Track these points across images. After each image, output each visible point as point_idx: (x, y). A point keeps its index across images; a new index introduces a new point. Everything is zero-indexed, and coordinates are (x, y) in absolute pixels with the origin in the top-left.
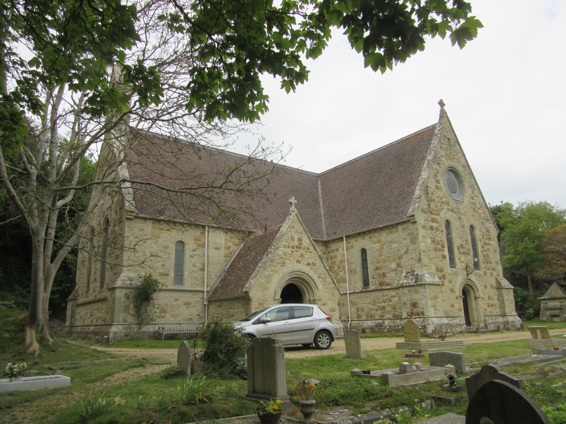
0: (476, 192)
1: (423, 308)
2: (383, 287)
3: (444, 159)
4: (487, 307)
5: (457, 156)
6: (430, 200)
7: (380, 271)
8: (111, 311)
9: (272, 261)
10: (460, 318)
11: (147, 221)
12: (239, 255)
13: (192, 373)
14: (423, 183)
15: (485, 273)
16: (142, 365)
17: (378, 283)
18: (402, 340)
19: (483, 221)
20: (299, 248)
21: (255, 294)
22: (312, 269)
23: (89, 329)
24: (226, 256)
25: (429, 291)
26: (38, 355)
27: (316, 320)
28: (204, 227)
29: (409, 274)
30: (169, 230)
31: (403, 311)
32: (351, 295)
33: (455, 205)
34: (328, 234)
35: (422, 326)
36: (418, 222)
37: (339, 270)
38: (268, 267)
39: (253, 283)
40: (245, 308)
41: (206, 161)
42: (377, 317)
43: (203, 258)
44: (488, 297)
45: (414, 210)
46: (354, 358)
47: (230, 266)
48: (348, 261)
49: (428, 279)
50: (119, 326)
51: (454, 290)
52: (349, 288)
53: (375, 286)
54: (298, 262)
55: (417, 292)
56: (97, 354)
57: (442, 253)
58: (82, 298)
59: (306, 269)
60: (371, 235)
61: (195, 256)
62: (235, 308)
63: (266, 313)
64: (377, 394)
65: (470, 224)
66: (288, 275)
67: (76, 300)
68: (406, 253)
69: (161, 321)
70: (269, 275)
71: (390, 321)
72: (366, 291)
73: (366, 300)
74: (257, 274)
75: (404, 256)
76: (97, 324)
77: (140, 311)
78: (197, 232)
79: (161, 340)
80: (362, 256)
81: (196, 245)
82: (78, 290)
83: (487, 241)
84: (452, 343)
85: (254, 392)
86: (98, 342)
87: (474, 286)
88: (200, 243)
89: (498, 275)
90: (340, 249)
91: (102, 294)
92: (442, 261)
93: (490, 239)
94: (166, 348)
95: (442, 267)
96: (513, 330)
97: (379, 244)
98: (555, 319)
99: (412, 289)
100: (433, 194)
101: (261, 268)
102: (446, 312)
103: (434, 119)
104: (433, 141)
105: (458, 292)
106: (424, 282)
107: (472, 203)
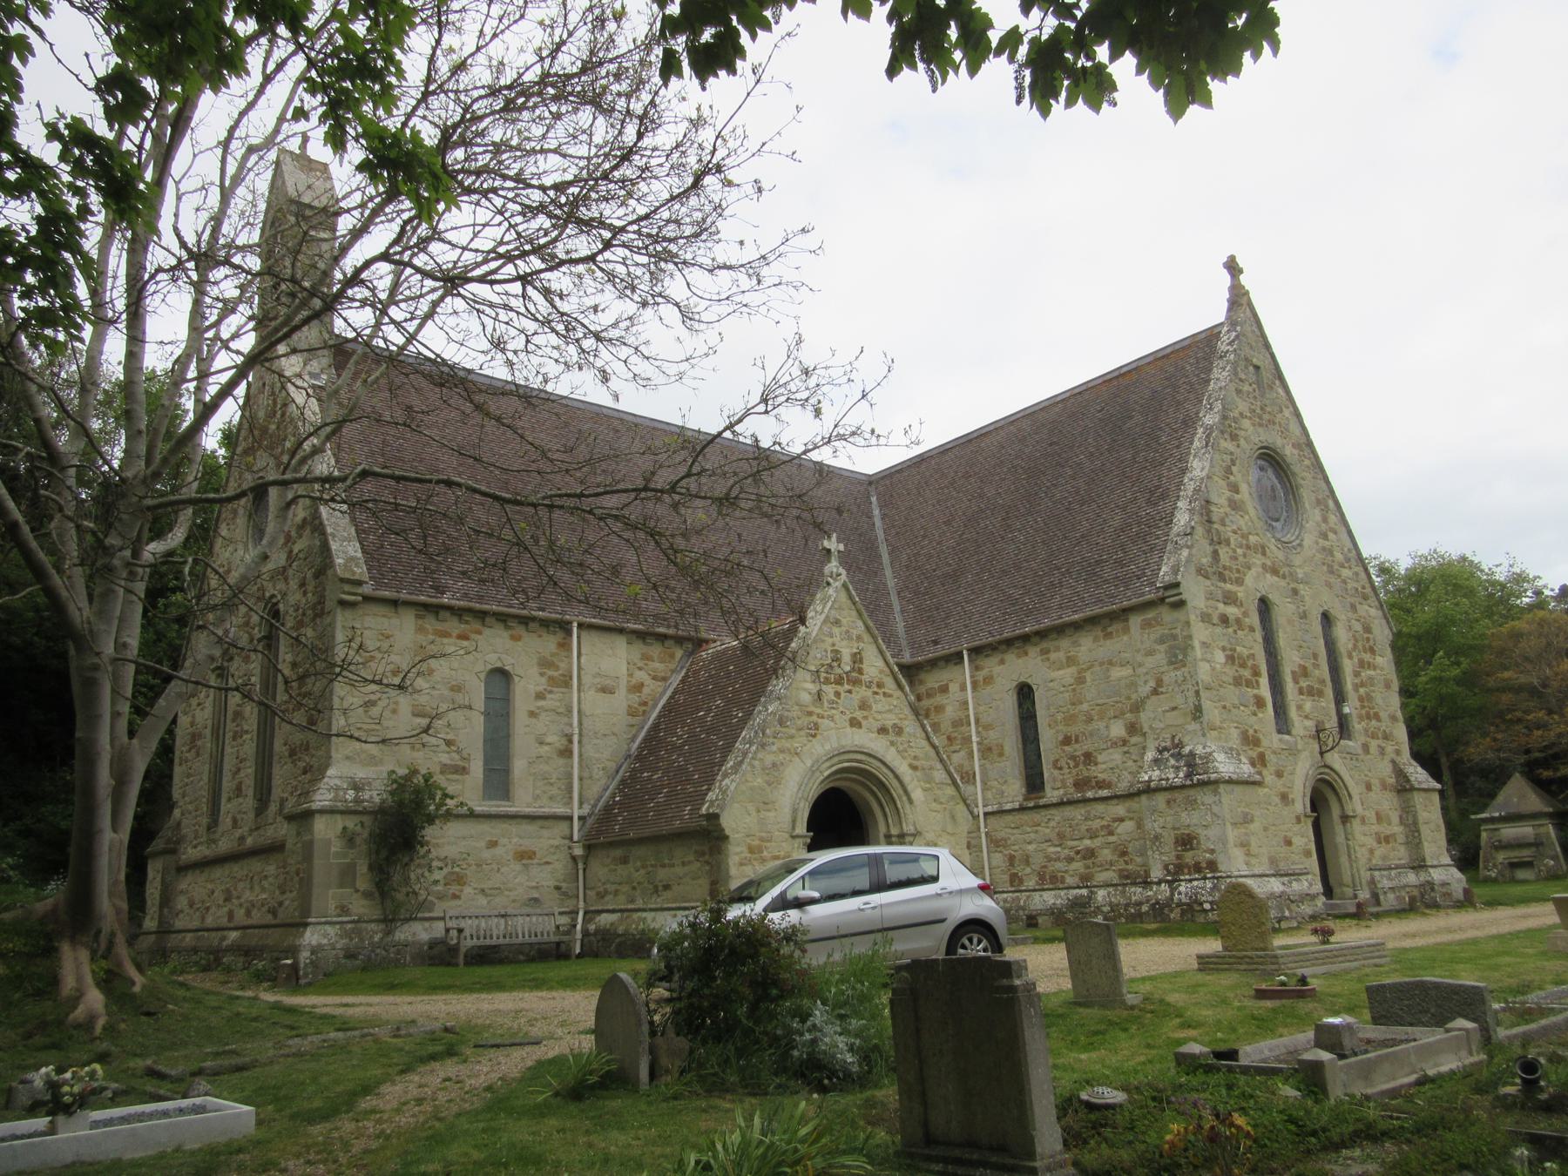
0: (1333, 519)
1: (1212, 851)
2: (1086, 792)
3: (1246, 423)
4: (1375, 844)
5: (1279, 416)
6: (1217, 541)
7: (1077, 746)
8: (302, 879)
9: (781, 722)
10: (1310, 877)
11: (401, 610)
12: (669, 708)
13: (653, 1075)
14: (1197, 491)
15: (1366, 748)
16: (451, 1052)
17: (1070, 781)
18: (1213, 945)
19: (1353, 600)
20: (856, 682)
21: (736, 821)
22: (892, 743)
23: (224, 938)
24: (632, 713)
25: (1229, 800)
26: (104, 1028)
27: (951, 893)
28: (565, 627)
29: (1166, 754)
30: (465, 638)
31: (1151, 861)
32: (991, 820)
33: (1280, 555)
34: (915, 646)
35: (1211, 903)
36: (1190, 604)
37: (952, 748)
38: (771, 740)
39: (732, 788)
40: (707, 863)
41: (556, 436)
42: (1070, 881)
43: (566, 719)
44: (1377, 814)
45: (1175, 570)
46: (1103, 1006)
47: (645, 740)
48: (977, 721)
49: (1224, 766)
50: (327, 927)
51: (1291, 796)
52: (984, 799)
53: (1062, 791)
54: (855, 723)
55: (1192, 804)
56: (288, 1019)
57: (1255, 691)
58: (195, 847)
59: (878, 745)
60: (1044, 645)
61: (544, 714)
62: (673, 866)
63: (803, 878)
64: (1324, 1130)
65: (1321, 610)
66: (828, 764)
67: (173, 852)
68: (1155, 692)
69: (452, 908)
70: (774, 765)
71: (1111, 889)
72: (1037, 807)
73: (1036, 832)
74: (741, 762)
75: (1149, 702)
76: (250, 922)
77: (388, 880)
78: (547, 644)
79: (457, 965)
80: (1020, 705)
81: (544, 680)
82: (179, 824)
83: (1367, 657)
84: (1358, 951)
85: (929, 1140)
86: (259, 977)
87: (1338, 785)
88: (556, 674)
89: (1398, 752)
90: (954, 687)
91: (261, 832)
92: (1255, 714)
93: (1372, 651)
94: (480, 990)
95: (1256, 731)
96: (1448, 907)
97: (1072, 670)
98: (1521, 874)
99: (1176, 795)
100: (1224, 525)
101: (751, 743)
102: (1273, 861)
103: (1213, 312)
104: (1216, 373)
105: (1301, 804)
106: (1214, 776)
107: (1324, 549)
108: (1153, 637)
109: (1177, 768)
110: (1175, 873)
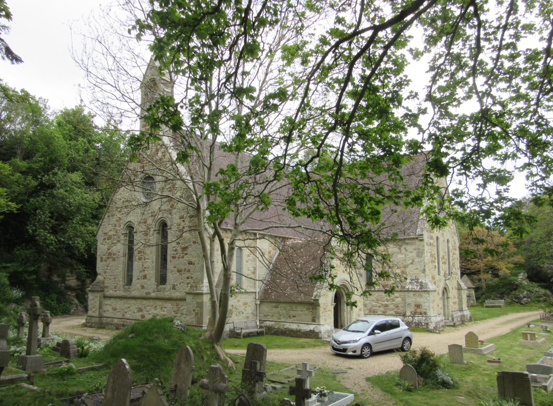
1: (426, 309)
29: (413, 281)
55: (421, 296)
68: (412, 263)
87: (447, 289)
99: (417, 293)
108: (412, 248)
109: (417, 286)
110: (414, 314)
